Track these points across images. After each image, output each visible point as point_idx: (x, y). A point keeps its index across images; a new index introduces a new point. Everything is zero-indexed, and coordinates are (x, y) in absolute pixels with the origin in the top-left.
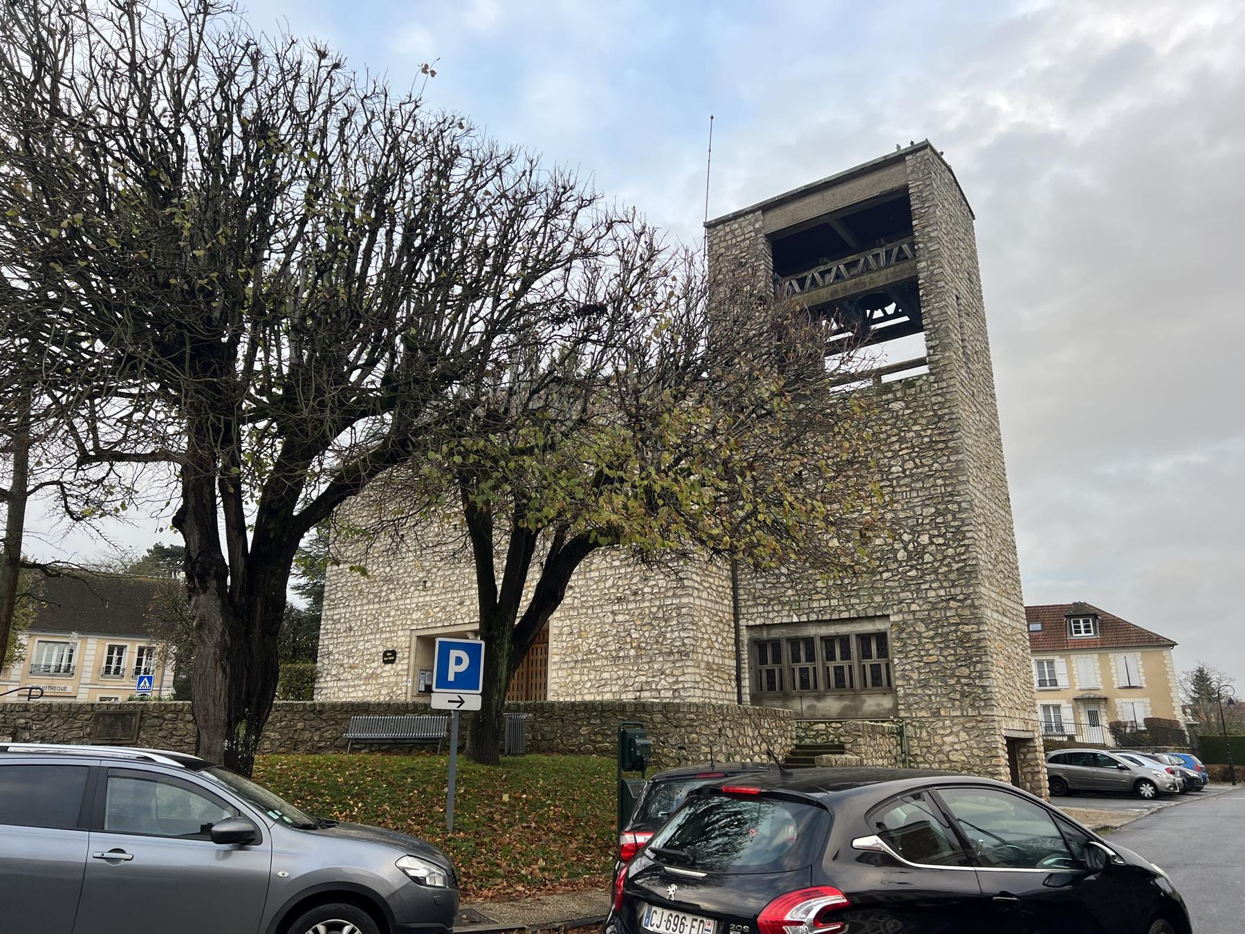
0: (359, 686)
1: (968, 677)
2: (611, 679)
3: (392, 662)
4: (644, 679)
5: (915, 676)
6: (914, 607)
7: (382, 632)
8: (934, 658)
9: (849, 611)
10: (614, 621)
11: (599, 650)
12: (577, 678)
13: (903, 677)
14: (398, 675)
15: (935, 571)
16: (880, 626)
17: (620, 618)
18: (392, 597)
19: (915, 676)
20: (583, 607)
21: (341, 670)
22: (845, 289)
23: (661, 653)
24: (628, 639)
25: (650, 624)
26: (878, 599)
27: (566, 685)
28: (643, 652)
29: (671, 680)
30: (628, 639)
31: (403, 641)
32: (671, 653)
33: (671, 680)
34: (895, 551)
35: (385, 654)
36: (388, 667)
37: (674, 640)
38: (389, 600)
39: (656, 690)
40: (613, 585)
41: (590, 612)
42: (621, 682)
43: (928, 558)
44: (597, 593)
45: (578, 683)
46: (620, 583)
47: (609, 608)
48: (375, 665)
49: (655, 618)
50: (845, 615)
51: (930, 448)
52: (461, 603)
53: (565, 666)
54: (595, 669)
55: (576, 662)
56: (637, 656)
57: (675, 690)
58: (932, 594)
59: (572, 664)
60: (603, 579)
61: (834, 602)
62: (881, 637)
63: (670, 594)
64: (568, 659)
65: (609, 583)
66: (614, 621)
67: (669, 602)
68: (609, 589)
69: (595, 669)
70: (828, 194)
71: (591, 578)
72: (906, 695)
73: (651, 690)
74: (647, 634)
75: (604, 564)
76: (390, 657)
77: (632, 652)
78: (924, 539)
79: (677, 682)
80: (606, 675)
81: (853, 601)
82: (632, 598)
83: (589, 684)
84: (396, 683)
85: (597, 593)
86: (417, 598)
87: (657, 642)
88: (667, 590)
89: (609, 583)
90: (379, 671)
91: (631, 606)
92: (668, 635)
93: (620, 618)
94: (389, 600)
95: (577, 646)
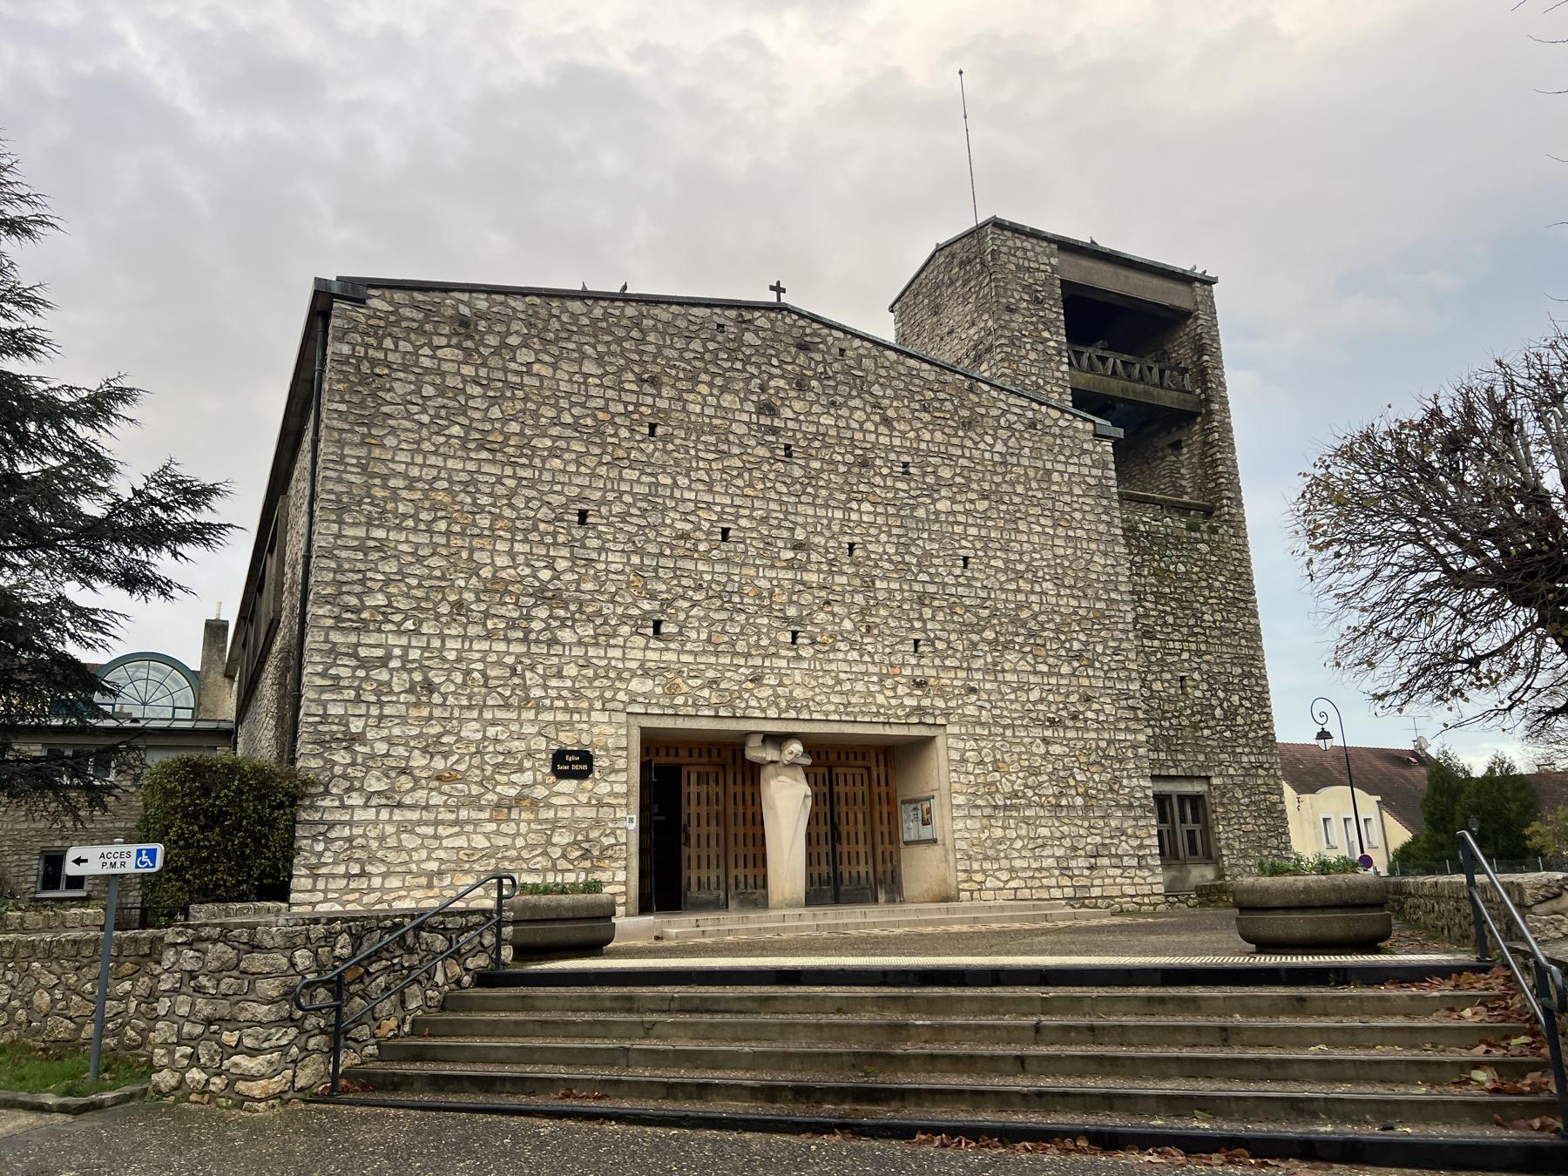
0: (477, 823)
1: (1277, 848)
2: (1052, 838)
3: (583, 776)
4: (1098, 839)
5: (1237, 845)
6: (1231, 771)
7: (539, 708)
8: (1250, 827)
9: (1176, 767)
10: (1048, 752)
11: (1030, 793)
12: (999, 833)
13: (1229, 846)
14: (600, 805)
15: (1246, 736)
16: (1198, 788)
17: (1056, 749)
18: (566, 635)
19: (1237, 845)
20: (996, 724)
21: (405, 783)
22: (1134, 392)
23: (1118, 805)
24: (1072, 782)
25: (1100, 763)
26: (1201, 757)
27: (981, 844)
28: (1094, 802)
29: (1135, 843)
30: (1072, 782)
31: (614, 741)
32: (1130, 806)
33: (1135, 843)
34: (1213, 708)
35: (559, 757)
36: (567, 786)
37: (1132, 789)
38: (553, 641)
39: (1117, 856)
40: (1042, 700)
41: (1009, 733)
42: (1067, 842)
43: (1240, 720)
44: (1017, 706)
45: (1000, 841)
46: (1051, 698)
47: (1037, 732)
48: (527, 777)
49: (1107, 757)
50: (1173, 772)
51: (1233, 604)
52: (757, 680)
53: (978, 813)
54: (1026, 821)
55: (995, 807)
56: (1086, 807)
57: (1140, 857)
58: (1245, 759)
59: (988, 811)
60: (1024, 687)
61: (1163, 756)
62: (1196, 800)
63: (1122, 726)
64: (980, 802)
65: (1034, 695)
66: (1048, 752)
67: (1121, 736)
68: (1034, 703)
69: (1026, 821)
70: (1086, 263)
71: (1005, 683)
72: (1231, 866)
73: (1110, 856)
74: (1096, 777)
75: (1023, 666)
76: (573, 764)
77: (1079, 801)
78: (1235, 699)
79: (1141, 846)
80: (1044, 832)
81: (1181, 757)
82: (1070, 724)
83: (1018, 844)
84: (598, 822)
85: (1017, 706)
86: (640, 651)
87: (1111, 790)
88: (1118, 720)
89: (1034, 695)
90: (540, 792)
91: (1071, 734)
92: (1125, 782)
93: (1056, 749)
94: (553, 641)
95: (993, 783)
